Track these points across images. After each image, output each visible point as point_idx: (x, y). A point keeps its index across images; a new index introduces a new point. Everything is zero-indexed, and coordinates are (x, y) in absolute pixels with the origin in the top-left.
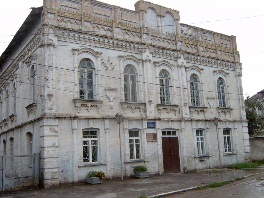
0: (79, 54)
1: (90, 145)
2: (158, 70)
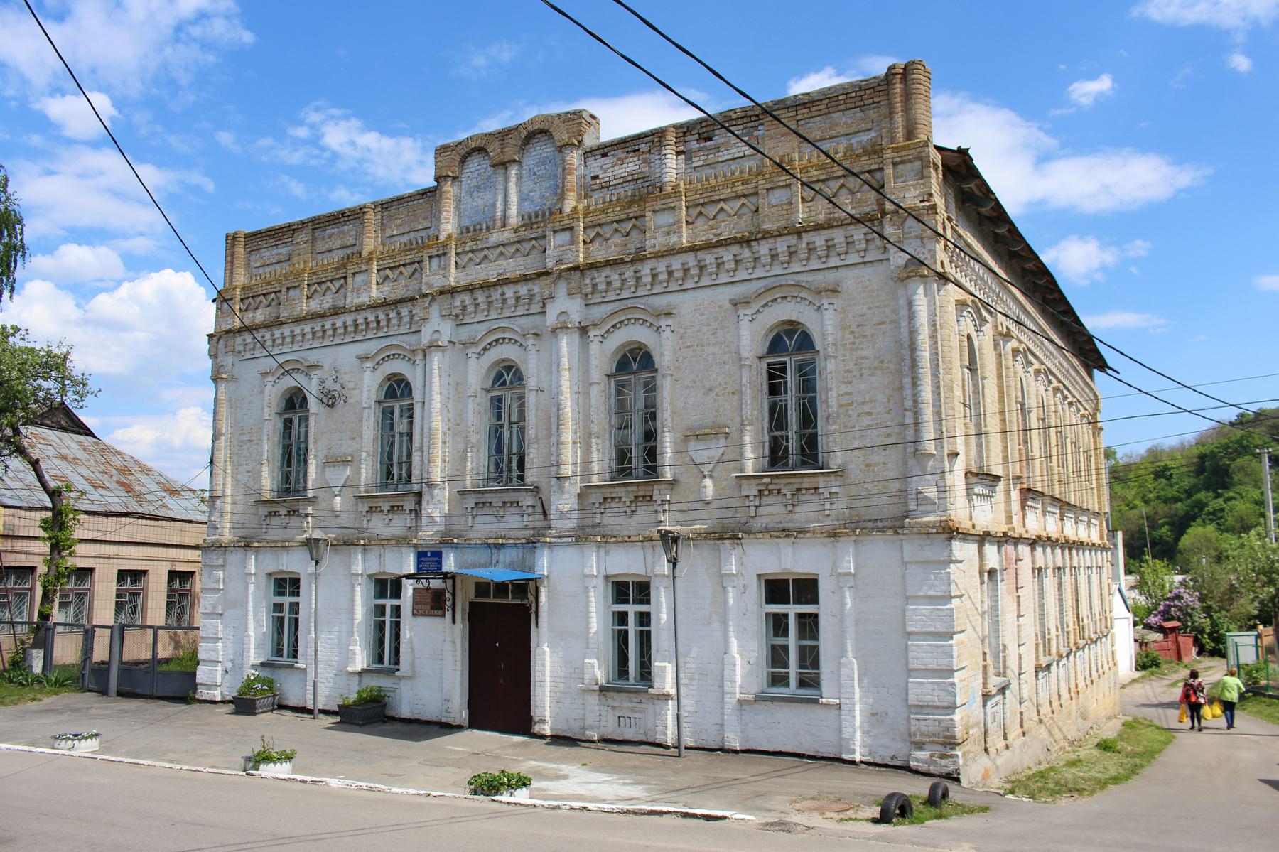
1: (632, 628)
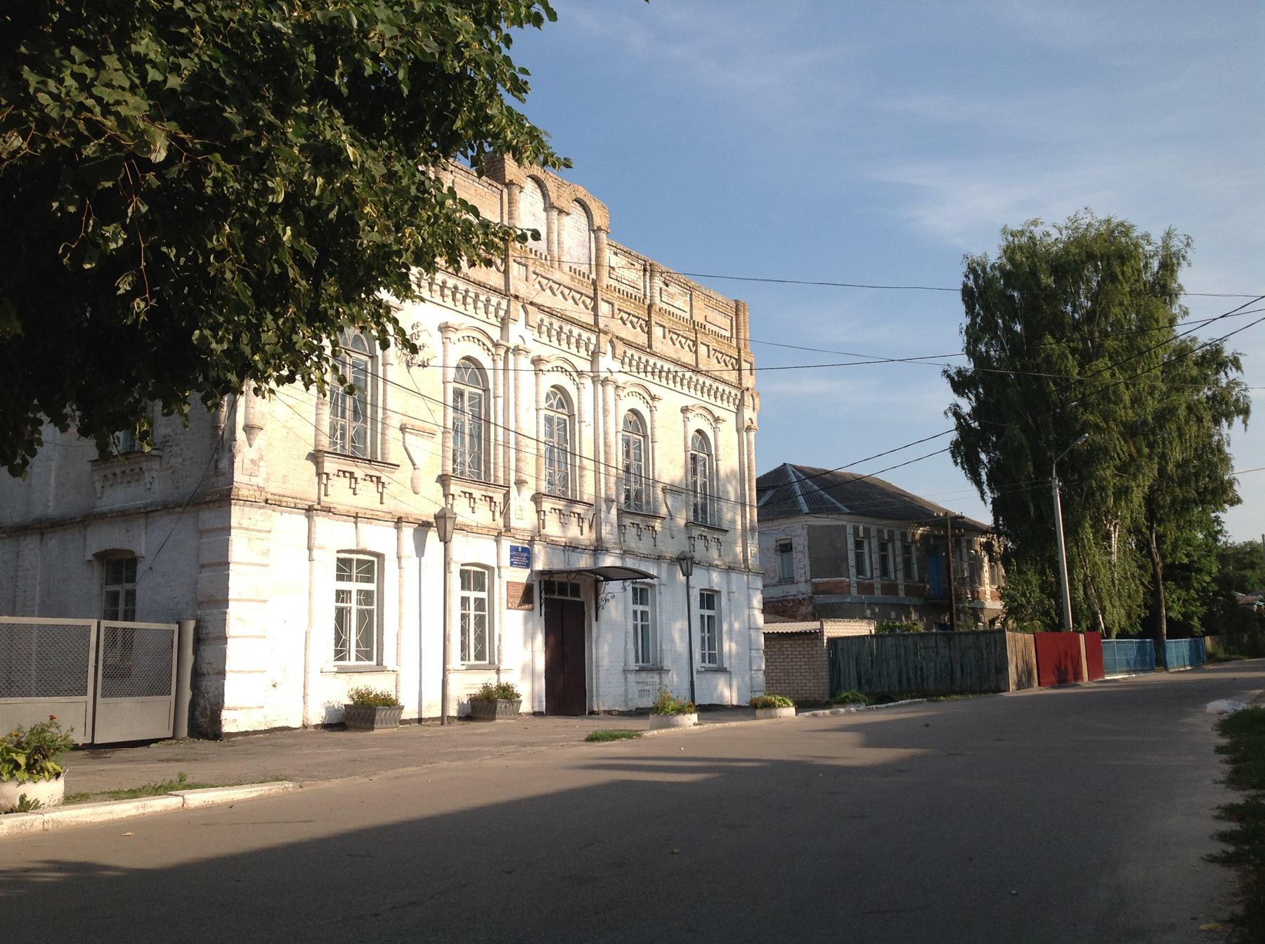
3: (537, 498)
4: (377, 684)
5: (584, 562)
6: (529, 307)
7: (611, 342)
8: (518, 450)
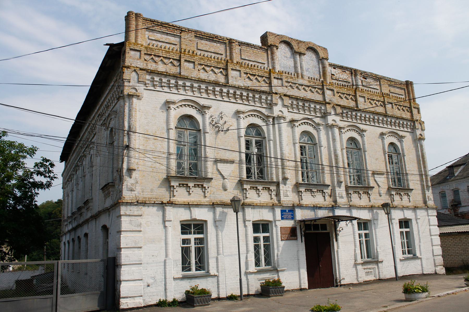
0: (176, 108)
2: (299, 130)
3: (347, 188)
4: (202, 284)
5: (321, 214)
6: (139, 72)
7: (333, 107)
8: (283, 169)
